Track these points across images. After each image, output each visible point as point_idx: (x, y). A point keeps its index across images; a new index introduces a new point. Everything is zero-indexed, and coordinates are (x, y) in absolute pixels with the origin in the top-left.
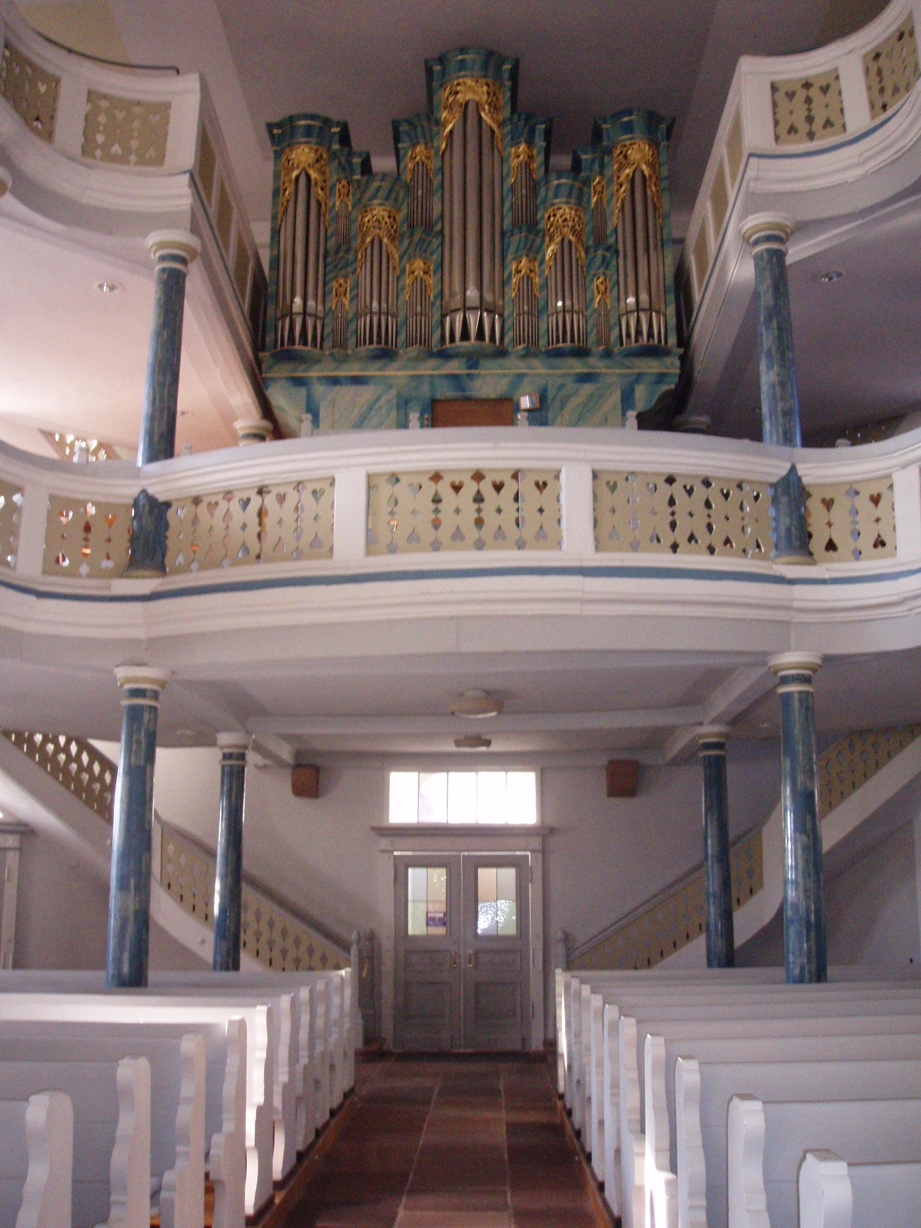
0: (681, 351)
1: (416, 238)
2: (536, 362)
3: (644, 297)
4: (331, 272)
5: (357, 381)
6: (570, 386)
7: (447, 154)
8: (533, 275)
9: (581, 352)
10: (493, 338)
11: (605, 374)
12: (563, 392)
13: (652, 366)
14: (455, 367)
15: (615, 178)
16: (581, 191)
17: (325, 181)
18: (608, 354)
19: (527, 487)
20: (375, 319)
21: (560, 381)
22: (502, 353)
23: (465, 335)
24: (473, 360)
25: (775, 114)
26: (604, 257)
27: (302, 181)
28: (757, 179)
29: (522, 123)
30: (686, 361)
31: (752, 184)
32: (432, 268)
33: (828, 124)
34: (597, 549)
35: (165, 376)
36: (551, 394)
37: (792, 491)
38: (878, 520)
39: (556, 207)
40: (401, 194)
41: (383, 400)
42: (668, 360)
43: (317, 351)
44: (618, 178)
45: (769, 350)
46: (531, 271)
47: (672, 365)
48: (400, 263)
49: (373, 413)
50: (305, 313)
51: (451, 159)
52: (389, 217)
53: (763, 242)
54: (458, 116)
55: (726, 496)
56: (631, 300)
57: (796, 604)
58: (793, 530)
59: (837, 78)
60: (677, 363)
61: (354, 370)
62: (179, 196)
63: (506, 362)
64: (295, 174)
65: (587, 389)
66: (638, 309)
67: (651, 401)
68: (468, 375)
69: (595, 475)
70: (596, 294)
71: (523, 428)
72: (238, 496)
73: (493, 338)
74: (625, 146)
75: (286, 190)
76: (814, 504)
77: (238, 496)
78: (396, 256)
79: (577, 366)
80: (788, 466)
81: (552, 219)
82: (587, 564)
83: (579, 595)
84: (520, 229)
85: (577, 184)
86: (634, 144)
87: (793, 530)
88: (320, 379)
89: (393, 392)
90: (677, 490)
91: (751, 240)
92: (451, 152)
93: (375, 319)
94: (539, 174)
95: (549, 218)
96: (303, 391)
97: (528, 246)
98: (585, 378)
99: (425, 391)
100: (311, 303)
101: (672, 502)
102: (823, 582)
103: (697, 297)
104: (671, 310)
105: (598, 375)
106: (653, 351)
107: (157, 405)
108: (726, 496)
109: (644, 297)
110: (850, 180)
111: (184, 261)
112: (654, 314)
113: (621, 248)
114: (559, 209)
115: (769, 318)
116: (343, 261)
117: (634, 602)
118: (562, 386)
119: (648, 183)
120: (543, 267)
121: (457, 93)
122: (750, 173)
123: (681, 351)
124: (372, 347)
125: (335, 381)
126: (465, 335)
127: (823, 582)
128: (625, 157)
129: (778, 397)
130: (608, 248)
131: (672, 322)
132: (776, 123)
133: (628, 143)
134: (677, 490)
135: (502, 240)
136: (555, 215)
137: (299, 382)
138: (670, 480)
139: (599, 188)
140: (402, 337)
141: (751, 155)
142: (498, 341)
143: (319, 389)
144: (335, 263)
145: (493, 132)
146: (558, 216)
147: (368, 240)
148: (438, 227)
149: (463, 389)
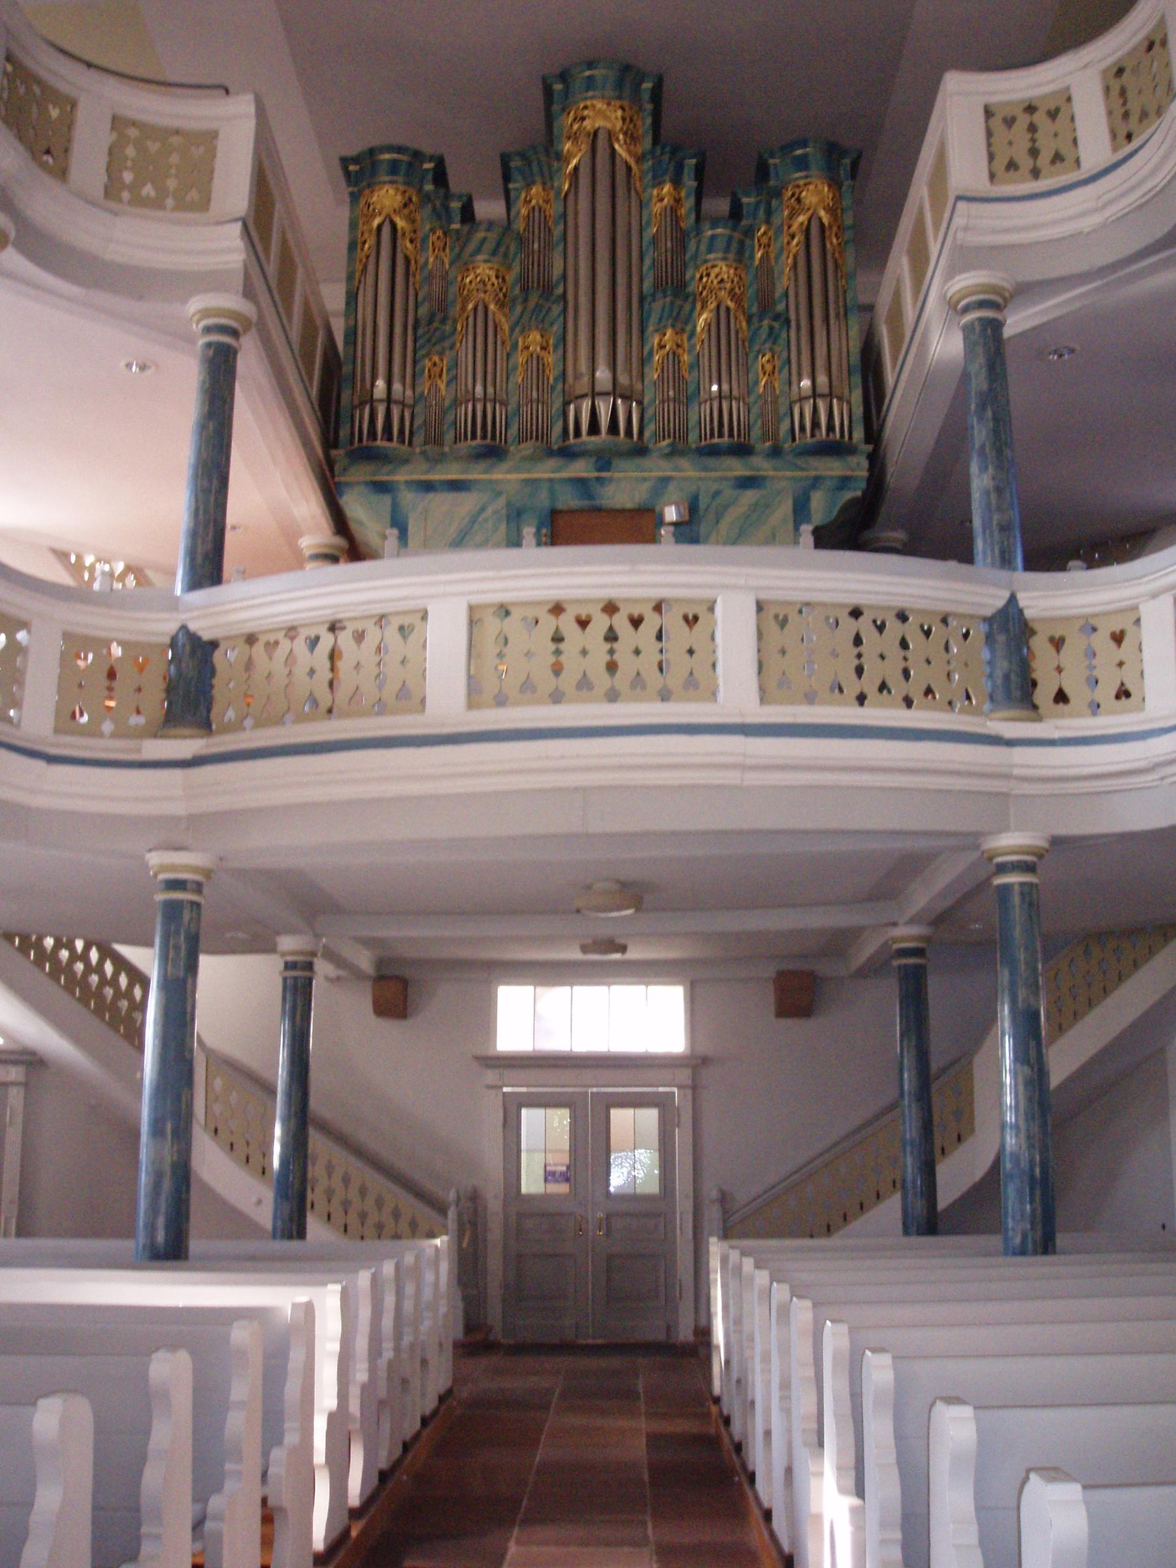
0: (870, 448)
1: (532, 304)
2: (684, 463)
3: (822, 379)
4: (422, 347)
5: (456, 486)
6: (728, 493)
7: (571, 197)
8: (680, 351)
9: (742, 450)
10: (629, 432)
11: (773, 478)
12: (718, 500)
13: (833, 468)
14: (581, 468)
15: (786, 228)
16: (742, 243)
17: (415, 232)
18: (776, 452)
19: (672, 621)
20: (479, 407)
21: (715, 487)
22: (641, 451)
23: (594, 428)
24: (604, 460)
25: (989, 145)
26: (771, 328)
27: (386, 231)
28: (966, 229)
29: (666, 157)
30: (876, 461)
31: (960, 235)
32: (551, 342)
33: (1058, 158)
34: (763, 701)
35: (210, 481)
36: (703, 502)
37: (1011, 627)
38: (1121, 664)
39: (709, 265)
40: (513, 248)
41: (489, 510)
42: (853, 460)
43: (404, 448)
44: (789, 227)
45: (982, 447)
46: (678, 346)
47: (858, 466)
48: (511, 335)
49: (476, 527)
50: (389, 400)
51: (576, 203)
52: (497, 277)
53: (974, 308)
54: (585, 148)
55: (927, 633)
56: (806, 383)
57: (1016, 772)
58: (1013, 676)
59: (1069, 99)
60: (865, 464)
61: (452, 473)
62: (229, 251)
63: (647, 462)
64: (376, 222)
65: (750, 496)
66: (815, 394)
67: (831, 512)
68: (598, 479)
69: (760, 607)
70: (761, 375)
71: (667, 546)
72: (304, 633)
73: (629, 432)
74: (798, 186)
75: (365, 242)
76: (1039, 644)
77: (304, 633)
78: (506, 327)
79: (737, 468)
80: (1006, 595)
81: (705, 280)
82: (749, 720)
83: (740, 759)
84: (664, 292)
85: (737, 236)
86: (810, 183)
87: (1013, 676)
88: (409, 484)
89: (502, 501)
90: (864, 625)
91: (959, 307)
92: (576, 194)
93: (479, 407)
94: (688, 222)
95: (701, 278)
96: (387, 499)
97: (675, 314)
98: (747, 483)
99: (543, 500)
100: (397, 386)
101: (858, 641)
102: (1051, 743)
103: (890, 379)
104: (857, 396)
105: (764, 478)
106: (834, 449)
107: (201, 517)
108: (927, 633)
109: (822, 379)
110: (1086, 230)
111: (235, 333)
112: (835, 401)
113: (793, 317)
114: (714, 266)
115: (982, 407)
116: (438, 334)
117: (809, 768)
118: (717, 493)
119: (827, 233)
120: (693, 342)
121: (583, 119)
122: (958, 221)
123: (870, 448)
124: (474, 443)
125: (428, 487)
126: (594, 428)
127: (1051, 743)
128: (799, 200)
129: (994, 507)
130: (776, 317)
131: (858, 411)
132: (991, 157)
133: (801, 182)
134: (864, 625)
135: (641, 307)
136: (708, 275)
137: (381, 487)
138: (856, 613)
139: (765, 240)
140: (513, 431)
141: (959, 198)
142: (635, 436)
143: (407, 497)
144: (427, 336)
145: (629, 169)
146: (713, 275)
147: (470, 306)
148: (559, 290)
149: (591, 497)
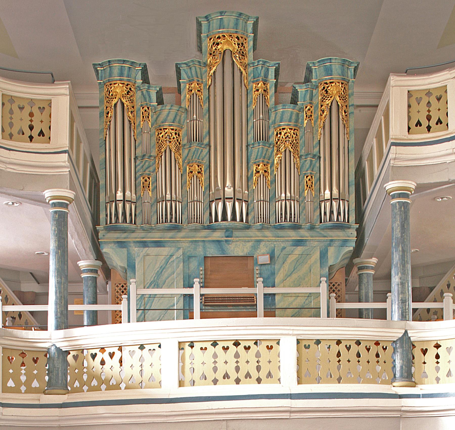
0: (357, 226)
1: (193, 149)
2: (267, 233)
3: (335, 191)
4: (139, 165)
5: (158, 244)
6: (289, 249)
7: (212, 87)
8: (267, 174)
9: (296, 227)
10: (242, 220)
11: (310, 241)
12: (284, 252)
13: (339, 235)
14: (218, 235)
15: (320, 106)
16: (298, 115)
17: (133, 107)
18: (312, 228)
19: (262, 348)
20: (169, 204)
21: (283, 245)
22: (248, 227)
23: (224, 218)
24: (229, 231)
25: (409, 112)
26: (311, 161)
27: (119, 106)
28: (395, 159)
29: (260, 67)
30: (360, 233)
31: (392, 162)
32: (203, 169)
33: (439, 122)
34: (299, 383)
35: (61, 278)
36: (277, 253)
37: (406, 343)
38: (449, 362)
39: (281, 128)
40: (183, 116)
41: (175, 257)
42: (350, 231)
43: (133, 226)
44: (322, 106)
45: (397, 264)
46: (265, 171)
47: (352, 234)
48: (183, 165)
49: (168, 266)
50: (124, 201)
51: (215, 89)
52: (176, 134)
53: (397, 198)
54: (219, 60)
55: (368, 350)
56: (328, 193)
57: (403, 409)
58: (404, 367)
59: (446, 92)
60: (355, 233)
61: (156, 236)
62: (65, 167)
63: (249, 233)
64: (115, 101)
65: (299, 250)
66: (331, 199)
67: (337, 258)
68: (226, 241)
69: (298, 341)
70: (306, 187)
71: (261, 320)
72: (108, 350)
73: (242, 220)
74: (326, 84)
75: (108, 113)
76: (417, 352)
77: (108, 350)
78: (181, 161)
79: (293, 235)
80: (403, 331)
81: (279, 136)
82: (293, 392)
83: (289, 409)
84: (259, 143)
85: (295, 111)
86: (332, 83)
87: (404, 367)
88: (134, 242)
89: (181, 252)
90: (342, 347)
91: (391, 194)
92: (215, 86)
93: (169, 204)
94: (271, 102)
95: (277, 135)
96: (125, 250)
97: (263, 155)
98: (299, 243)
99: (200, 251)
100: (128, 193)
101: (339, 355)
102: (418, 396)
103: (368, 193)
104: (352, 198)
105: (306, 241)
106: (339, 227)
107: (58, 295)
108: (368, 350)
109: (335, 191)
110: (448, 162)
111: (66, 206)
112: (341, 201)
113: (322, 155)
114: (284, 129)
115: (397, 245)
116: (147, 164)
117: (414, 80)
118: (284, 248)
119: (340, 110)
120: (272, 168)
121: (218, 44)
122: (391, 156)
123: (357, 226)
124: (167, 225)
125: (144, 244)
126: (224, 218)
127: (418, 396)
128: (327, 91)
129: (400, 292)
130: (314, 156)
131: (353, 206)
132: (409, 118)
133: (328, 82)
134: (342, 347)
135: (247, 149)
136: (280, 133)
137: (121, 244)
138: (339, 342)
139: (309, 114)
140: (185, 217)
141: (393, 144)
142: (244, 221)
143: (135, 250)
144: (141, 165)
145: (241, 73)
146: (283, 134)
147: (163, 150)
148: (206, 141)
149: (223, 250)
